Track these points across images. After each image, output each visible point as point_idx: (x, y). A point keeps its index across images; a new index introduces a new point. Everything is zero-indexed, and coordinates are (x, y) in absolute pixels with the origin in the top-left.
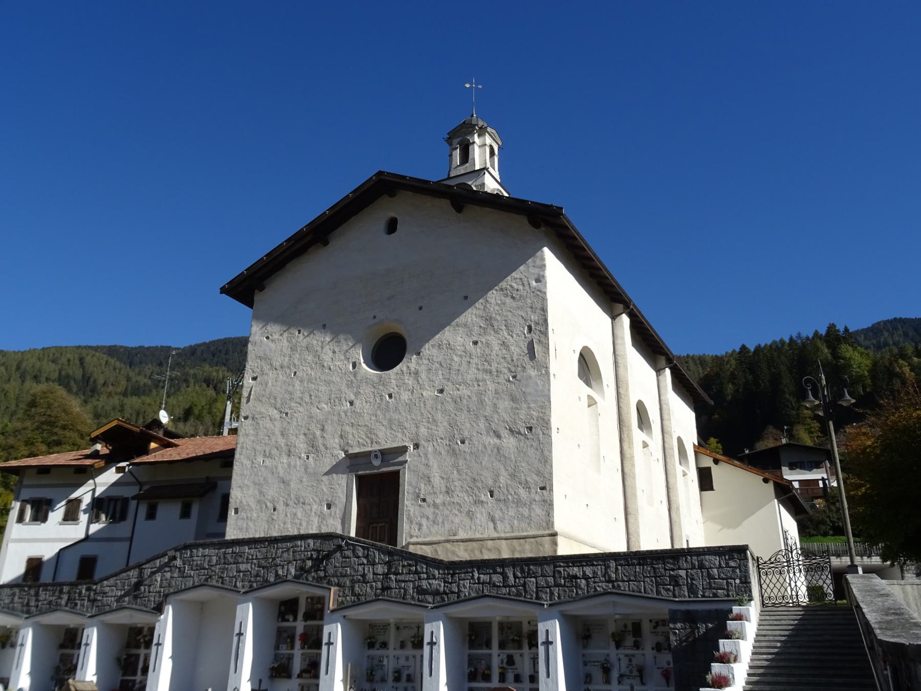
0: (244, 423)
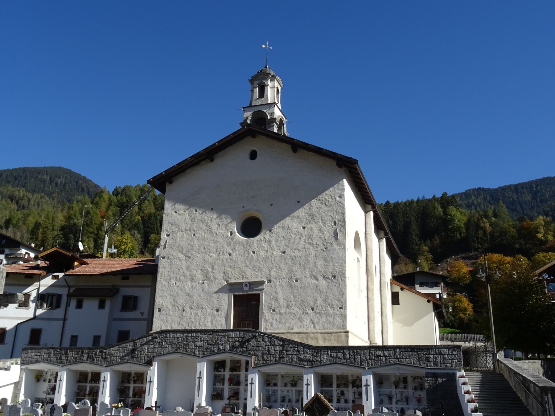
0: (162, 261)
